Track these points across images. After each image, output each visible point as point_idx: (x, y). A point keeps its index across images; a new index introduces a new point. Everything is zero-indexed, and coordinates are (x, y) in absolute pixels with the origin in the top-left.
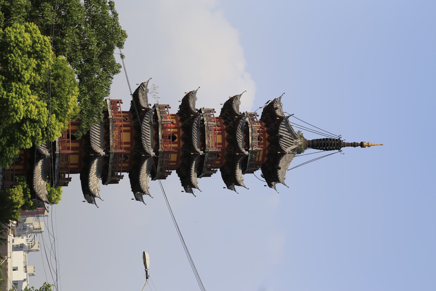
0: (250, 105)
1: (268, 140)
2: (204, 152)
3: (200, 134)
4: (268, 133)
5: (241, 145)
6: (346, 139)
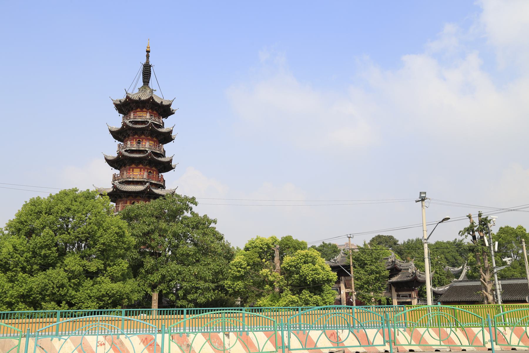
2: (148, 182)
6: (144, 61)
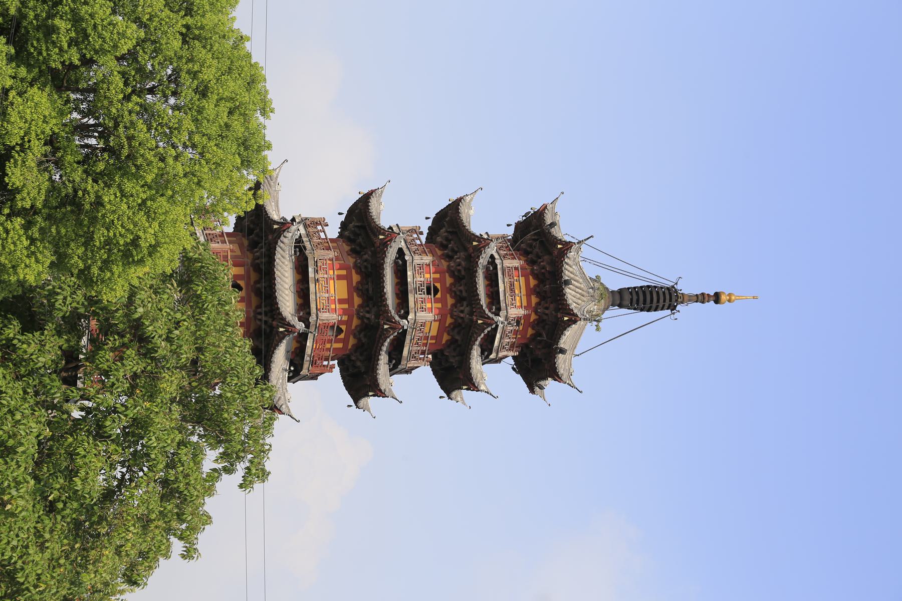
0: (491, 219)
1: (450, 290)
3: (299, 277)
4: (452, 275)
5: (483, 301)
6: (685, 288)
